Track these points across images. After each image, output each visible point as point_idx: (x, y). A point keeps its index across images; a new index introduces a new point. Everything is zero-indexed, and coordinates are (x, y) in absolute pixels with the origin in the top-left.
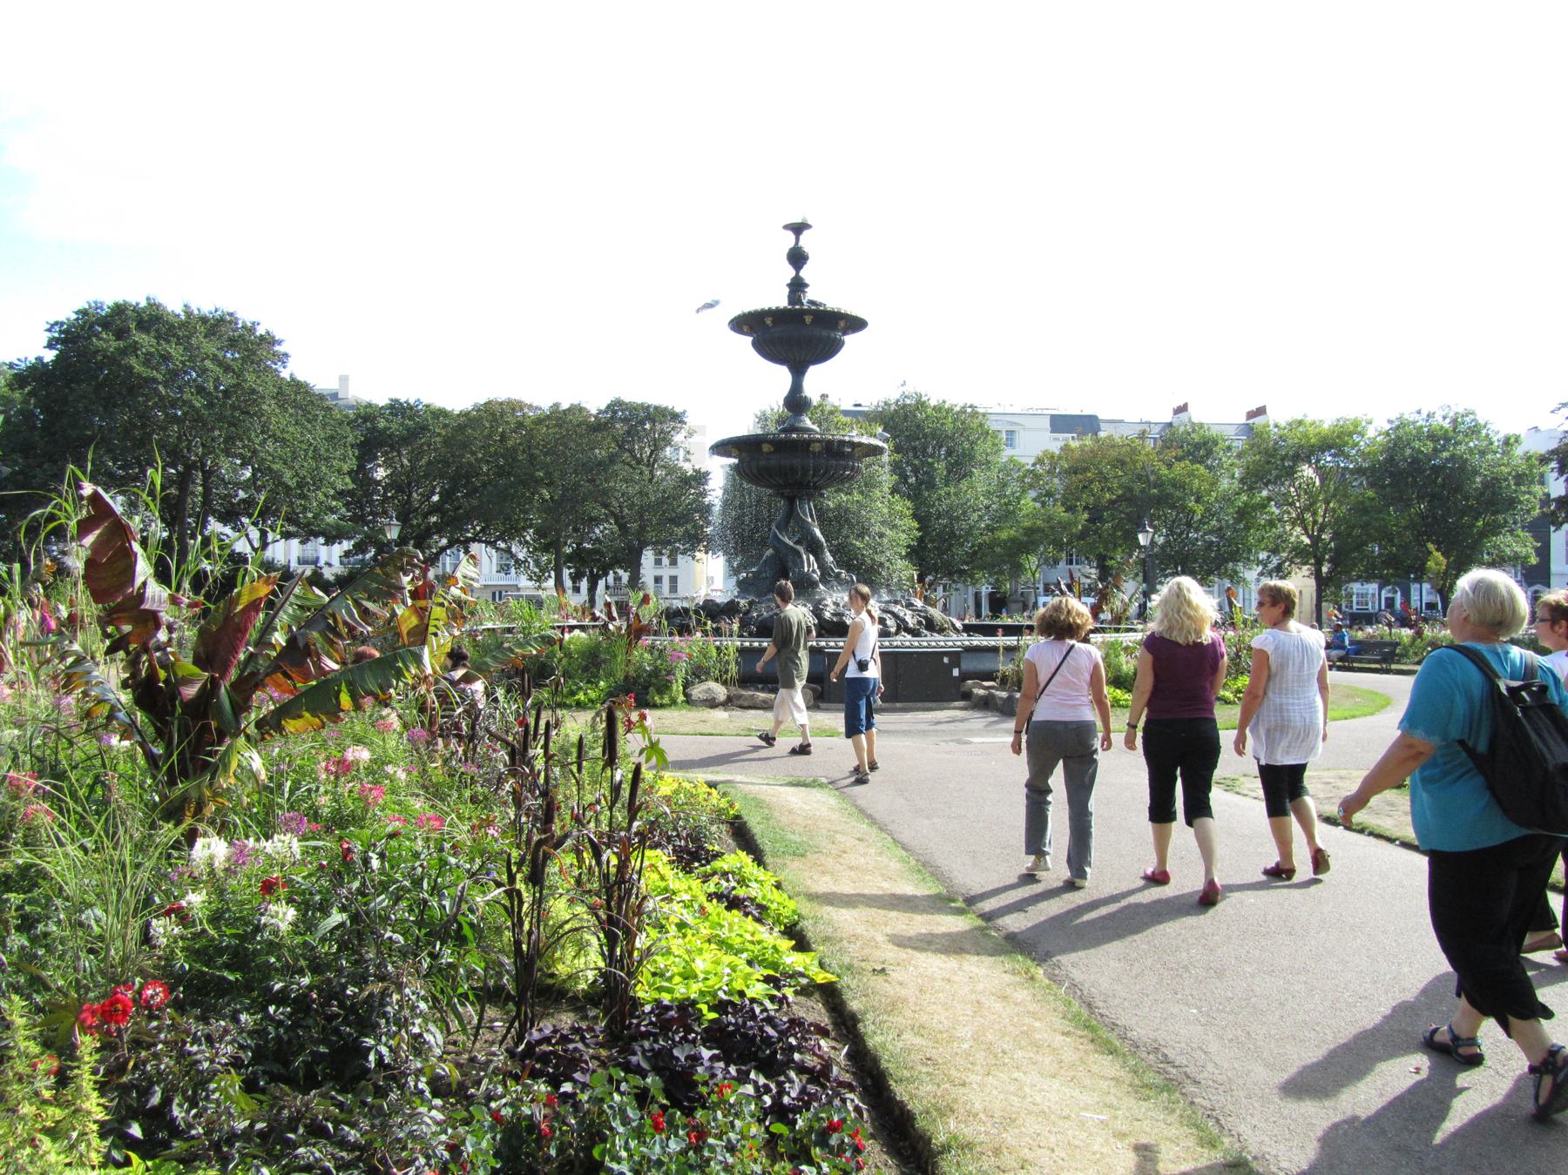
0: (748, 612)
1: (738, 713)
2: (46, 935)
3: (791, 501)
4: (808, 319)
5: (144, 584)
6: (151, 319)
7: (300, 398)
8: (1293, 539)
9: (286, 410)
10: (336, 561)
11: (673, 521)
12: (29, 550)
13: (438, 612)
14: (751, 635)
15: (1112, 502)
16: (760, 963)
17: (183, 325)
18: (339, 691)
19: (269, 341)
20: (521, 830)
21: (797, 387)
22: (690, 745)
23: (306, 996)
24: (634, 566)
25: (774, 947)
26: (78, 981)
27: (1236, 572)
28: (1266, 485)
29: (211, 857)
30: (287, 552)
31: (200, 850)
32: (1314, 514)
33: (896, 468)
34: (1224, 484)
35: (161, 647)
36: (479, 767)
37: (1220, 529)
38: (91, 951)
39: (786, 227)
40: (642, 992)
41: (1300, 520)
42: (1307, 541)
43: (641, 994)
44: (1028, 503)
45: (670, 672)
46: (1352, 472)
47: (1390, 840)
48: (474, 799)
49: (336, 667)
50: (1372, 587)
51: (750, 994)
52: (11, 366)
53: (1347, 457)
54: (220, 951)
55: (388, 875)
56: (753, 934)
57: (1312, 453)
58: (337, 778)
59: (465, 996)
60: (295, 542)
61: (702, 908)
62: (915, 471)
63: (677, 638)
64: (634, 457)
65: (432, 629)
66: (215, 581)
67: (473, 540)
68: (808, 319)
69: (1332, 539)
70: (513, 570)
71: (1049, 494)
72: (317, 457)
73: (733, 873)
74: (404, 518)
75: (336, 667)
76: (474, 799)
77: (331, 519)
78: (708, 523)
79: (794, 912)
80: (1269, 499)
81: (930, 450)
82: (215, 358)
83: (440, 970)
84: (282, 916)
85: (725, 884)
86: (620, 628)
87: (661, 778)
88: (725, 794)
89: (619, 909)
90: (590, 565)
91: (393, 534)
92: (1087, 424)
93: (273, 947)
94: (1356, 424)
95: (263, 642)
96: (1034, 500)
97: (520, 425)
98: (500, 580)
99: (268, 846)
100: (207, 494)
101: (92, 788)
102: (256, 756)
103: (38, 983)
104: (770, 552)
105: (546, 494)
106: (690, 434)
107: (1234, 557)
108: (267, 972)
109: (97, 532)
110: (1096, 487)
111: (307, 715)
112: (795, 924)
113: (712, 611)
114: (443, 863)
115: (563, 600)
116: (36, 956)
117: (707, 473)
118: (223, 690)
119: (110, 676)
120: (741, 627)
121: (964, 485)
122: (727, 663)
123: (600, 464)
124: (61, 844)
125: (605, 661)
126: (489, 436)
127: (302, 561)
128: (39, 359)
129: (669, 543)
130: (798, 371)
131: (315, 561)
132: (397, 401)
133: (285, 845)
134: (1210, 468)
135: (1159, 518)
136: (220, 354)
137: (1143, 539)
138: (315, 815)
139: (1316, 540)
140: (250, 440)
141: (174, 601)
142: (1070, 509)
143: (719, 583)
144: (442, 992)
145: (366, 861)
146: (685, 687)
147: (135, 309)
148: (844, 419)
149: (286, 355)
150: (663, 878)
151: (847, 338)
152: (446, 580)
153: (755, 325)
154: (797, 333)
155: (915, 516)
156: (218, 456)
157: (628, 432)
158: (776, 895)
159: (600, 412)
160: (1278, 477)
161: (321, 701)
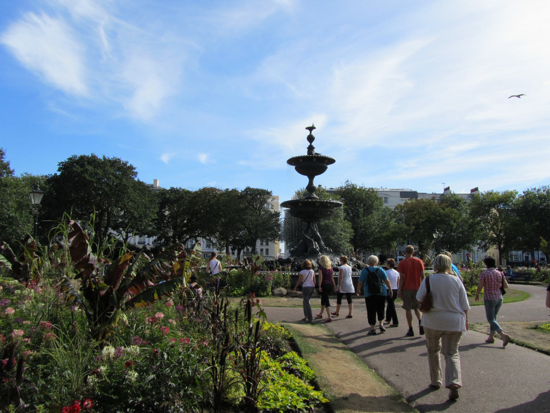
0: (294, 262)
1: (291, 299)
2: (51, 380)
3: (309, 223)
4: (315, 160)
5: (89, 255)
6: (92, 161)
7: (141, 187)
8: (490, 235)
9: (136, 192)
10: (151, 243)
11: (267, 230)
12: (50, 240)
13: (187, 263)
14: (295, 270)
15: (423, 222)
16: (302, 395)
17: (103, 163)
18: (154, 293)
19: (131, 168)
20: (216, 343)
21: (311, 183)
22: (278, 312)
23: (141, 405)
24: (254, 246)
25: (307, 389)
26: (61, 397)
27: (469, 247)
28: (479, 216)
29: (109, 353)
30: (135, 240)
31: (105, 351)
32: (497, 226)
33: (346, 210)
34: (464, 215)
35: (94, 277)
36: (201, 319)
37: (463, 232)
38: (66, 386)
39: (307, 128)
40: (259, 405)
41: (492, 229)
42: (495, 236)
43: (259, 406)
44: (393, 223)
45: (267, 284)
46: (510, 211)
47: (534, 349)
48: (199, 331)
49: (152, 284)
50: (520, 252)
51: (298, 407)
52: (46, 176)
53: (508, 205)
54: (111, 388)
55: (170, 361)
56: (299, 384)
57: (495, 204)
58: (152, 323)
59: (196, 405)
60: (137, 237)
61: (280, 373)
62: (352, 212)
63: (269, 272)
64: (254, 207)
65: (185, 269)
66: (112, 252)
67: (198, 236)
68: (315, 160)
69: (504, 235)
70: (211, 247)
71: (400, 220)
72: (146, 207)
73: (291, 360)
74: (174, 228)
75: (152, 284)
76: (199, 331)
77: (150, 228)
78: (280, 230)
79: (313, 375)
80: (481, 221)
81: (357, 204)
82: (113, 174)
83: (187, 396)
84: (133, 375)
85: (288, 364)
86: (249, 268)
87: (264, 323)
88: (287, 330)
89: (251, 372)
90: (238, 245)
91: (171, 234)
92: (413, 195)
93: (129, 386)
94: (511, 193)
95: (128, 275)
96: (395, 222)
97: (215, 196)
98: (207, 250)
99: (128, 349)
100: (108, 220)
101: (68, 326)
102: (125, 316)
103: (48, 398)
104: (301, 241)
105: (224, 220)
106: (273, 199)
107: (469, 242)
108: (126, 396)
109: (74, 237)
110: (417, 217)
111: (142, 301)
112: (314, 379)
113: (281, 261)
114: (189, 356)
115: (229, 258)
116: (47, 388)
117: (279, 213)
118: (114, 292)
119: (75, 284)
120: (291, 268)
121: (370, 217)
122: (287, 280)
123: (242, 210)
124: (58, 347)
125: (244, 280)
126: (204, 200)
127: (139, 243)
128: (56, 174)
129: (266, 237)
130: (311, 179)
131: (144, 243)
132: (173, 188)
133: (135, 349)
134: (458, 210)
135: (440, 228)
136: (115, 173)
137: (435, 236)
138: (143, 336)
139: (498, 236)
140: (123, 201)
141: (99, 260)
142: (408, 225)
143: (283, 251)
144: (188, 404)
145: (162, 355)
146: (272, 289)
147: (88, 157)
148: (327, 194)
149: (137, 173)
150: (266, 361)
151: (328, 166)
152: (190, 251)
153: (296, 162)
154: (311, 164)
155: (353, 228)
156: (113, 207)
157: (252, 199)
158: (307, 369)
159: (242, 192)
160: (483, 213)
161: (147, 296)
